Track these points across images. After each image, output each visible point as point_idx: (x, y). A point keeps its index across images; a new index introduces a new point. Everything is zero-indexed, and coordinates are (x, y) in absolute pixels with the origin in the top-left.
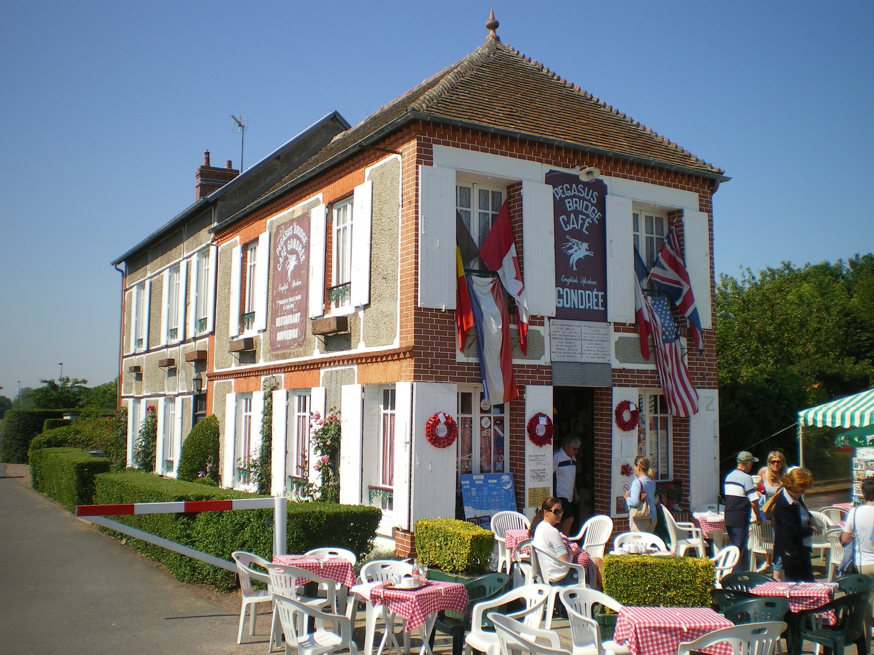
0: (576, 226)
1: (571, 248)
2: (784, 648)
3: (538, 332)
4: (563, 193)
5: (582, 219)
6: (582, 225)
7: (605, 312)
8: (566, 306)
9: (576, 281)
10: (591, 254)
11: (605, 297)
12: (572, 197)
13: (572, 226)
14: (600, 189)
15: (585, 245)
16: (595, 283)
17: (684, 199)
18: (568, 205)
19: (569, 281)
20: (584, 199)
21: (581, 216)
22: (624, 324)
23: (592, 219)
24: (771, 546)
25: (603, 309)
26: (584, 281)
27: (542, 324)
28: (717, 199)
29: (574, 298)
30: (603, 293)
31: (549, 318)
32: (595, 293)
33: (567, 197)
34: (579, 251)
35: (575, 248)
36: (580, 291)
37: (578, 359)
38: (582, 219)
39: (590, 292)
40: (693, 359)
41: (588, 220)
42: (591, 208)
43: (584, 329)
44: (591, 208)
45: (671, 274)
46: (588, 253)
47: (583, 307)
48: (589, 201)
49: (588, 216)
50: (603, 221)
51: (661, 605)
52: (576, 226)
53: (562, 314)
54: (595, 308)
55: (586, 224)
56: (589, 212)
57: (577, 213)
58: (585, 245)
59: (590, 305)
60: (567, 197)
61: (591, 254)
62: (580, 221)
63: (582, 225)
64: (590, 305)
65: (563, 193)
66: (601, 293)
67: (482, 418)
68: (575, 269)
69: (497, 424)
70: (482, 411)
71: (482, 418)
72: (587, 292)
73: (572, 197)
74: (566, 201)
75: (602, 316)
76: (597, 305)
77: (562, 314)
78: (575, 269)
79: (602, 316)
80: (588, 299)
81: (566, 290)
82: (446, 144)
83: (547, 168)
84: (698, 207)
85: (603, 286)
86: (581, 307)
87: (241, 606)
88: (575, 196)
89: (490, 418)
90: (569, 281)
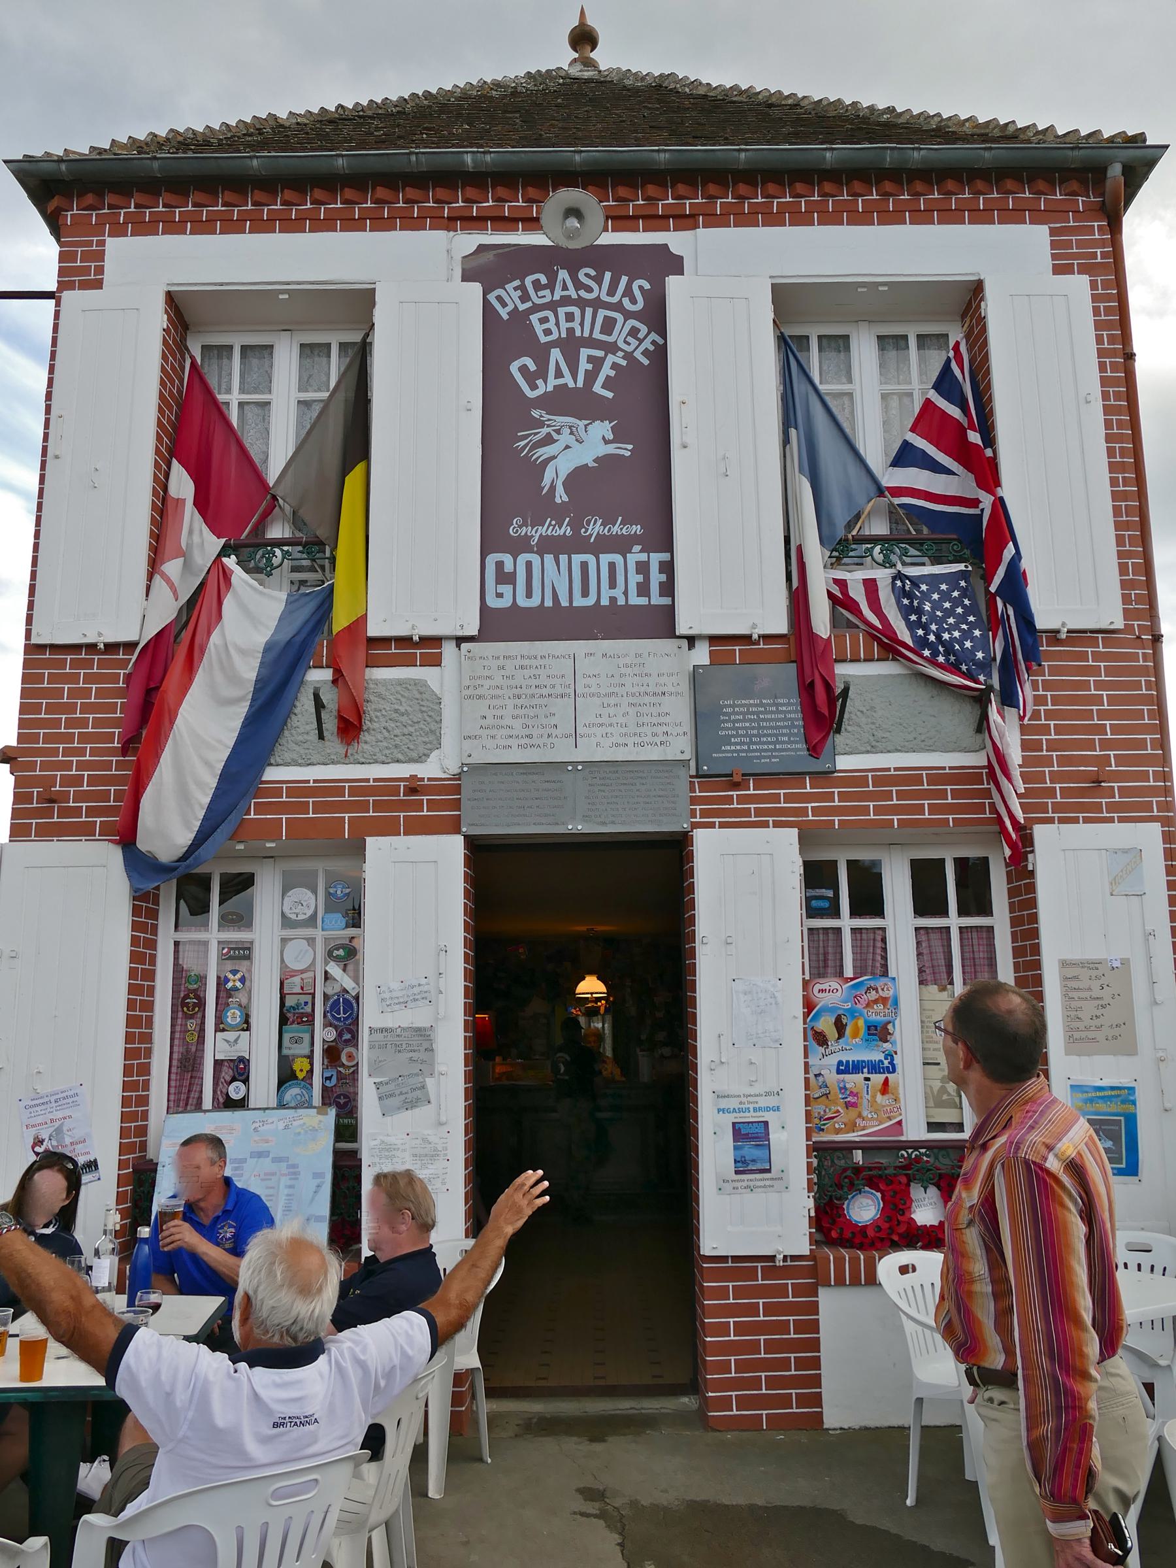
0: (568, 379)
1: (548, 440)
3: (421, 685)
4: (525, 298)
5: (590, 359)
6: (591, 377)
7: (669, 613)
8: (522, 602)
9: (565, 530)
10: (625, 450)
11: (668, 568)
12: (553, 306)
13: (552, 382)
15: (602, 429)
16: (637, 529)
17: (1008, 258)
18: (539, 329)
19: (536, 533)
20: (597, 304)
21: (585, 353)
22: (746, 639)
23: (628, 356)
25: (666, 601)
26: (595, 528)
27: (436, 661)
28: (1142, 227)
29: (553, 580)
31: (460, 640)
33: (536, 308)
34: (578, 447)
35: (565, 438)
36: (577, 559)
37: (563, 753)
38: (590, 359)
39: (617, 558)
40: (1037, 746)
41: (611, 359)
42: (623, 327)
43: (583, 666)
44: (623, 327)
45: (956, 482)
46: (611, 449)
47: (590, 601)
48: (618, 307)
49: (612, 348)
50: (660, 355)
52: (568, 379)
53: (497, 625)
54: (635, 600)
55: (606, 371)
56: (619, 335)
57: (571, 346)
58: (602, 429)
59: (618, 593)
60: (536, 308)
61: (625, 450)
62: (584, 366)
63: (591, 377)
64: (613, 593)
65: (525, 298)
66: (656, 558)
67: (284, 941)
68: (561, 496)
69: (337, 959)
70: (286, 922)
71: (284, 941)
72: (605, 559)
73: (553, 306)
74: (534, 318)
75: (662, 623)
76: (643, 589)
77: (497, 625)
78: (561, 496)
79: (662, 623)
80: (618, 579)
81: (523, 558)
82: (144, 228)
83: (468, 241)
84: (1048, 263)
86: (579, 601)
88: (566, 301)
89: (311, 941)
90: (536, 533)
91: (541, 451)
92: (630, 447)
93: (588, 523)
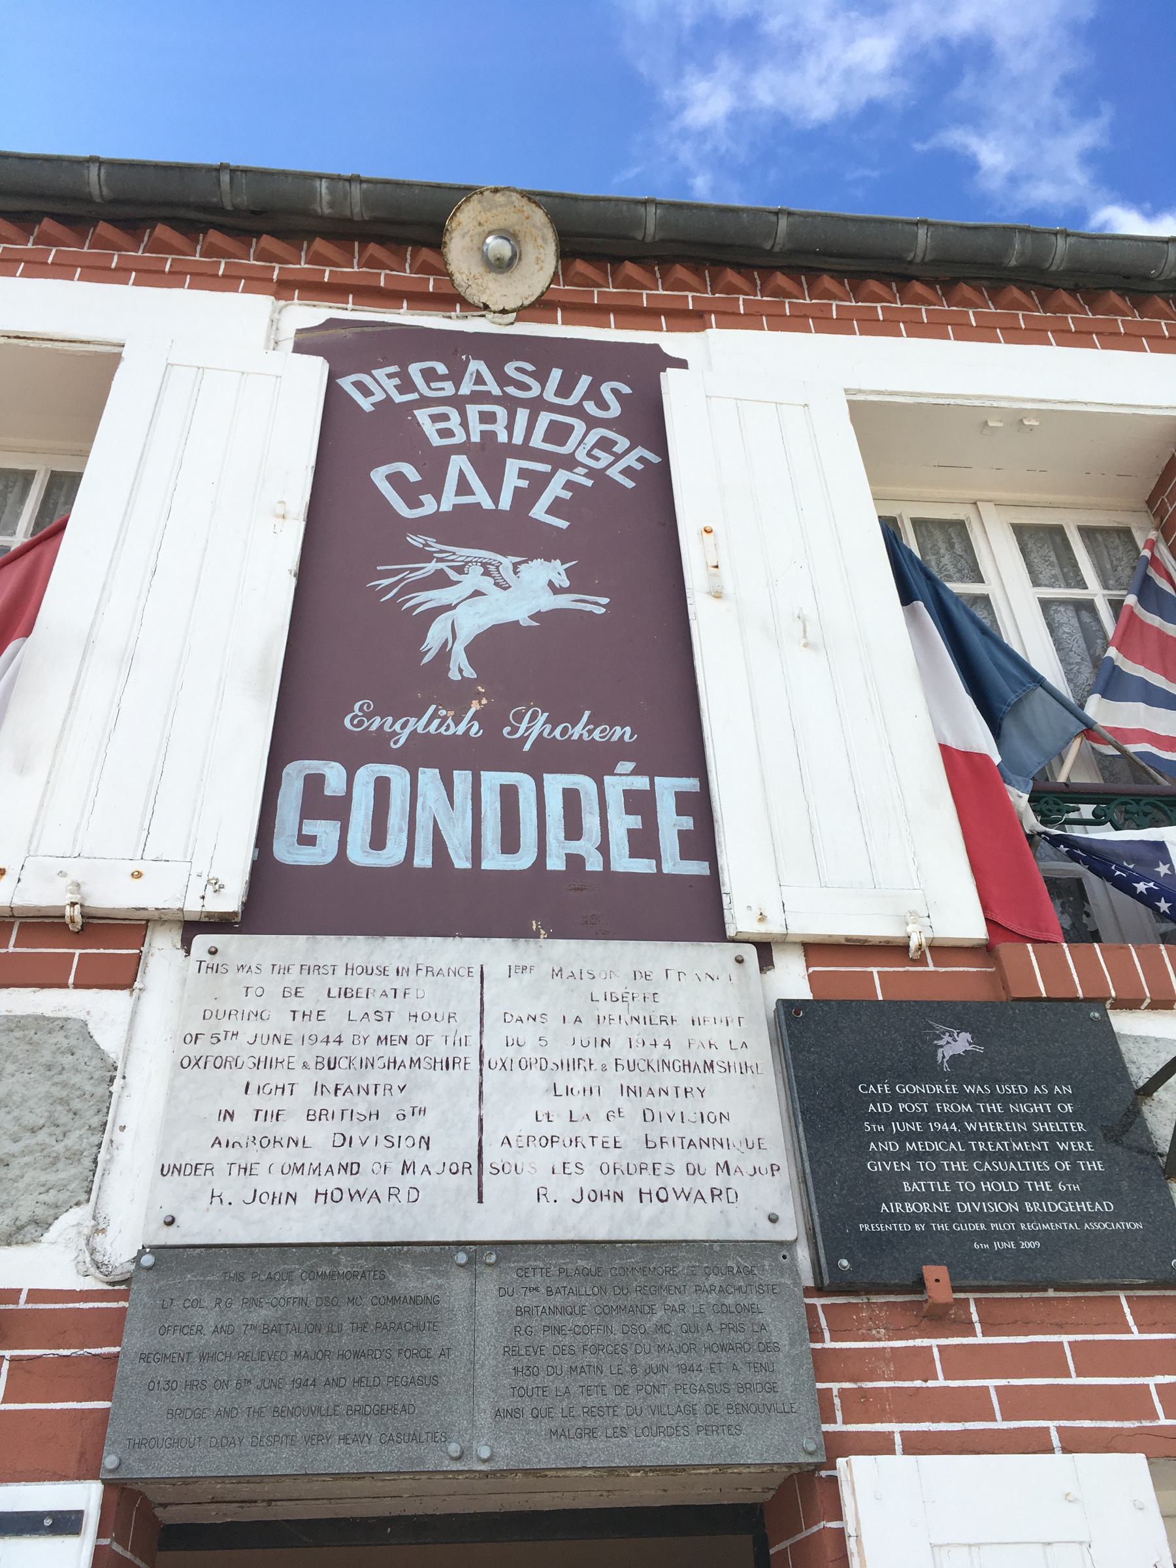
1: (440, 581)
2: (626, 390)
7: (710, 890)
11: (699, 806)
14: (577, 273)
24: (327, 211)
30: (690, 784)
31: (192, 927)
32: (616, 786)
35: (474, 579)
46: (565, 602)
47: (523, 860)
50: (658, 481)
51: (1058, 902)
53: (276, 899)
59: (587, 847)
60: (424, 402)
76: (644, 842)
79: (691, 910)
83: (310, 314)
85: (678, 740)
86: (494, 860)
87: (1156, 824)
91: (422, 596)
92: (605, 601)
93: (519, 717)
